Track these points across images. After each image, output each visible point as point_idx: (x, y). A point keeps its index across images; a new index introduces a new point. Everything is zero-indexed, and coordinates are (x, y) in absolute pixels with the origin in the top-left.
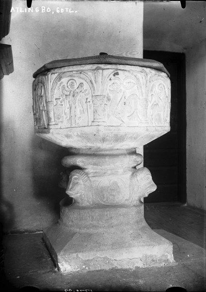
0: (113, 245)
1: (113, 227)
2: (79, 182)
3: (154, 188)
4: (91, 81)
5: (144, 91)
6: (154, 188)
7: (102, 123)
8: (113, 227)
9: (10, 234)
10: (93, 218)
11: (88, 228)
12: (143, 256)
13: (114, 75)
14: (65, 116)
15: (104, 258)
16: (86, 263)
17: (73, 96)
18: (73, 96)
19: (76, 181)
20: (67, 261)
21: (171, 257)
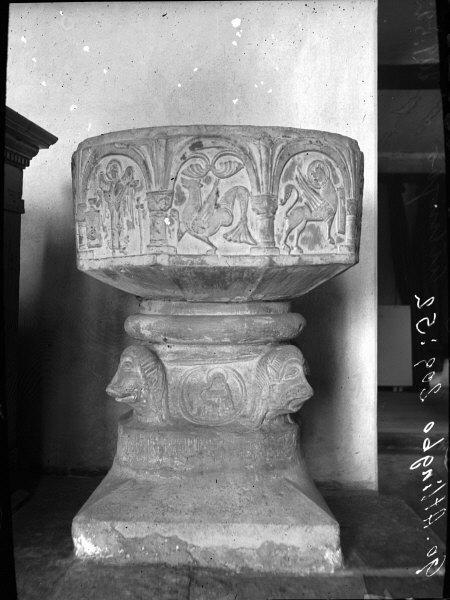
0: (195, 511)
1: (202, 473)
2: (133, 370)
3: (411, 384)
4: (145, 163)
5: (262, 178)
6: (411, 384)
8: (202, 473)
9: (70, 476)
10: (162, 449)
11: (152, 472)
12: (263, 545)
13: (192, 148)
14: (103, 234)
15: (169, 538)
16: (125, 543)
18: (116, 192)
19: (127, 369)
20: (90, 536)
21: (333, 557)
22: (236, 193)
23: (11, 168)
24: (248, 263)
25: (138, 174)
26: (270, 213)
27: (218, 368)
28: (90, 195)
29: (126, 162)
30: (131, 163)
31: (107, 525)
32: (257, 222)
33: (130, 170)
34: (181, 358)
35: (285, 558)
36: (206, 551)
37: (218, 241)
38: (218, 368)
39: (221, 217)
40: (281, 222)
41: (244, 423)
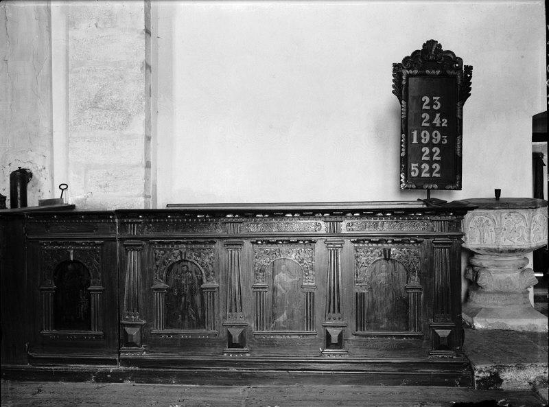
22: (521, 227)
23: (159, 197)
24: (524, 247)
25: (491, 222)
26: (529, 233)
27: (508, 275)
28: (470, 226)
29: (486, 219)
30: (488, 219)
31: (484, 319)
32: (526, 236)
33: (487, 221)
34: (496, 272)
35: (130, 115)
36: (512, 326)
37: (515, 241)
38: (508, 275)
39: (516, 234)
40: (532, 235)
41: (517, 291)
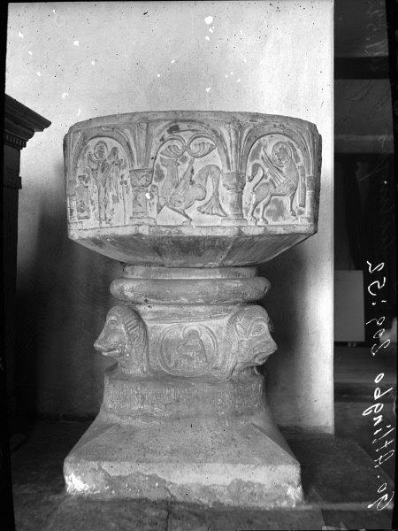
0: (173, 452)
1: (178, 419)
2: (118, 327)
3: (363, 340)
4: (128, 144)
5: (232, 158)
6: (363, 340)
7: (146, 221)
8: (178, 419)
9: (62, 421)
10: (143, 398)
11: (134, 418)
13: (170, 131)
14: (91, 207)
15: (150, 476)
16: (110, 481)
17: (103, 170)
18: (103, 170)
19: (112, 327)
20: (80, 474)
21: (294, 493)
22: (209, 170)
24: (220, 233)
25: (122, 154)
26: (239, 188)
27: (193, 326)
28: (80, 172)
29: (111, 143)
30: (116, 144)
31: (94, 464)
32: (228, 196)
33: (115, 150)
34: (160, 317)
36: (182, 488)
37: (192, 213)
38: (193, 326)
39: (195, 192)
40: (248, 197)
41: (216, 374)
